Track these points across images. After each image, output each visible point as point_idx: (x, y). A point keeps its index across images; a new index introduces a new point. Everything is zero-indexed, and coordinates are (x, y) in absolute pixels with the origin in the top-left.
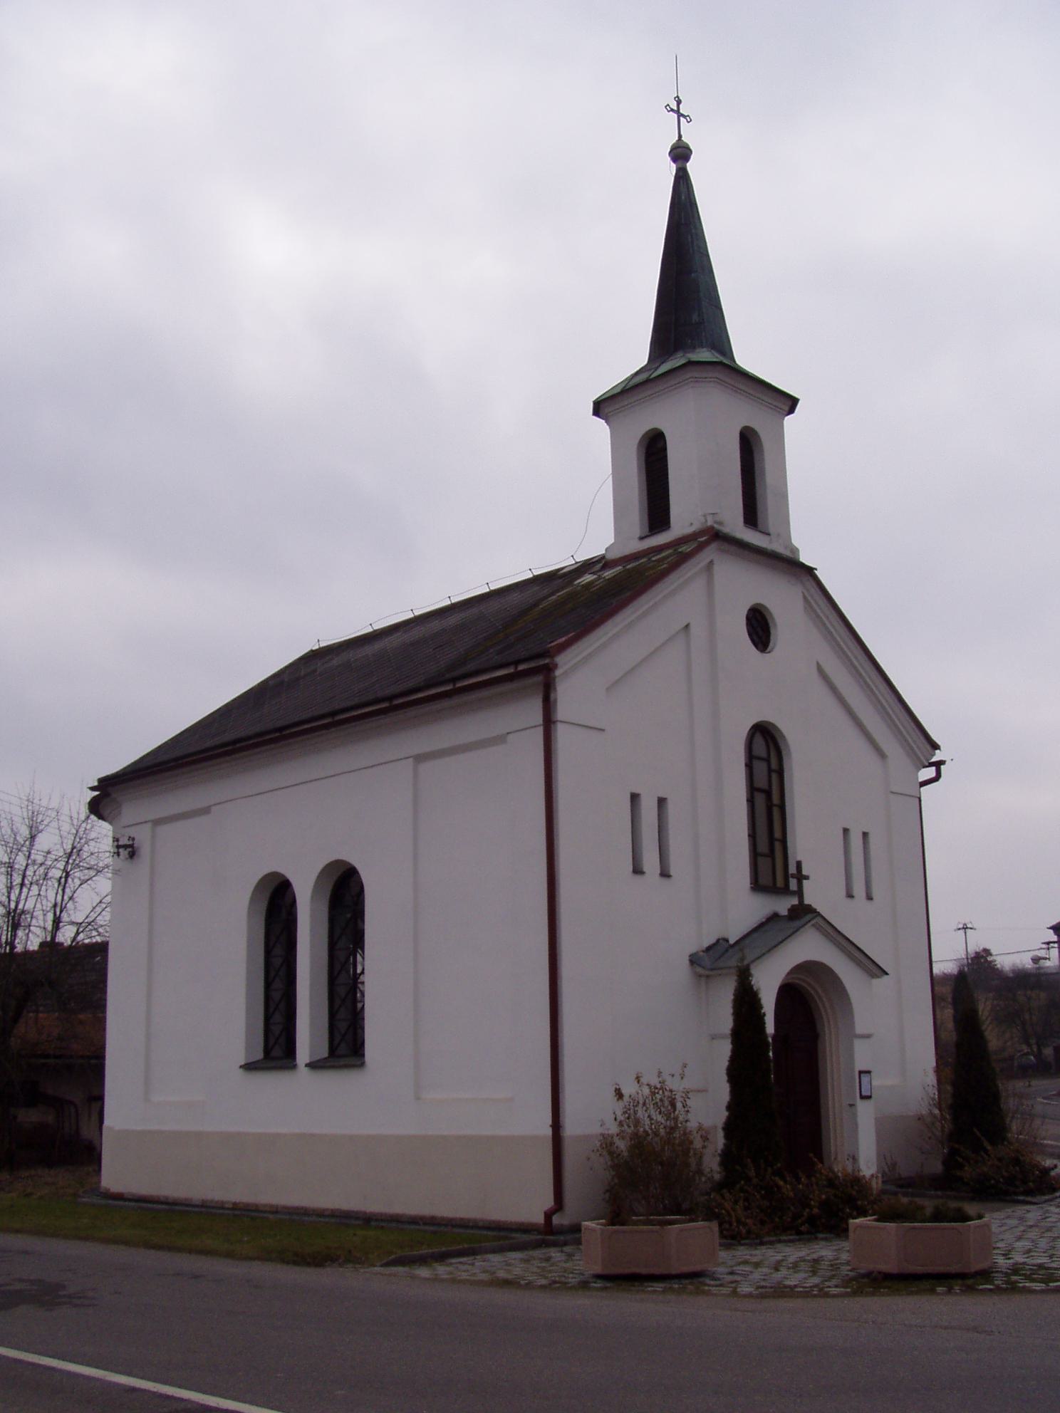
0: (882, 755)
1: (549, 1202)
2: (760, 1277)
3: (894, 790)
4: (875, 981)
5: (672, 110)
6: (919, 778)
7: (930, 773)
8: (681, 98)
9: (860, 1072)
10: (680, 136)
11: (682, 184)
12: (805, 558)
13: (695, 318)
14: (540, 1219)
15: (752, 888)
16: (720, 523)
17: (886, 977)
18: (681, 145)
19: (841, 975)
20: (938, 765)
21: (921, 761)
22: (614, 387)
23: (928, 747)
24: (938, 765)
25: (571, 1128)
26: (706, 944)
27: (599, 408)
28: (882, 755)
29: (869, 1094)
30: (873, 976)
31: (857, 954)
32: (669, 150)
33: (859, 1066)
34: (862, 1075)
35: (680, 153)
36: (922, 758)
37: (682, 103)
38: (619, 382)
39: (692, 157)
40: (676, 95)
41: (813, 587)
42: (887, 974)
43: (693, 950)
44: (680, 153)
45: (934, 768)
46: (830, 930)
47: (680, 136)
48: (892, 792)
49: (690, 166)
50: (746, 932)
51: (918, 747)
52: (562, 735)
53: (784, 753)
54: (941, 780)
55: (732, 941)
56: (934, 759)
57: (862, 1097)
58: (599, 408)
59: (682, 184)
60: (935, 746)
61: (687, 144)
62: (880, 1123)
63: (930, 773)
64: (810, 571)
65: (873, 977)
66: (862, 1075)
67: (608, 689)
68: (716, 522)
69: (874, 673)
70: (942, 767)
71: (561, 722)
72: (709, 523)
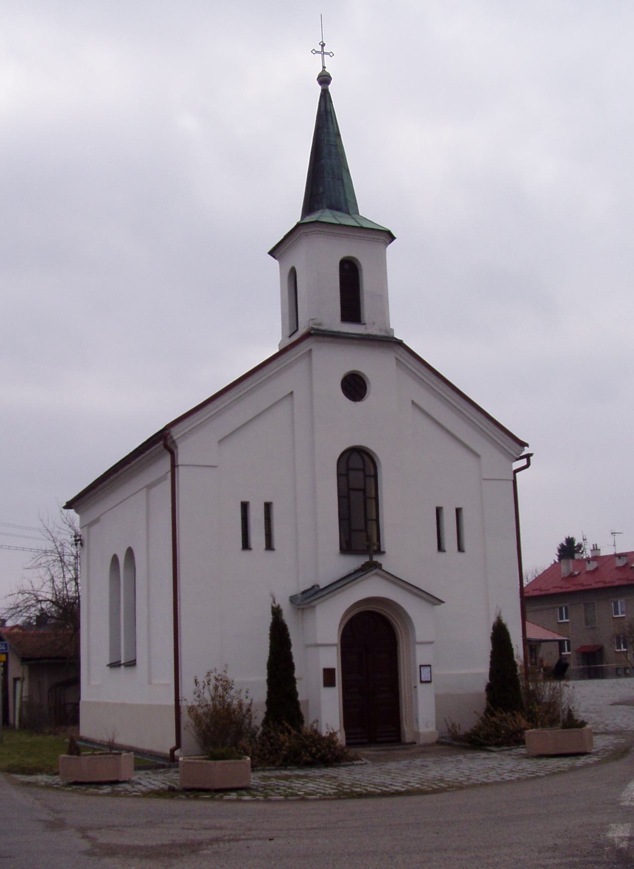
0: (477, 455)
1: (173, 743)
2: (537, 768)
3: (485, 477)
4: (436, 607)
5: (317, 52)
6: (513, 467)
7: (523, 462)
8: (324, 42)
9: (421, 666)
10: (324, 67)
11: (325, 97)
12: (397, 336)
13: (321, 190)
14: (168, 752)
15: (340, 553)
16: (320, 324)
17: (443, 604)
18: (324, 74)
19: (403, 605)
20: (528, 456)
21: (514, 457)
22: (366, 219)
23: (518, 447)
24: (528, 456)
25: (183, 704)
26: (303, 589)
27: (272, 253)
28: (477, 455)
29: (429, 680)
30: (435, 604)
31: (415, 591)
32: (317, 77)
33: (420, 660)
34: (422, 668)
35: (324, 80)
36: (513, 453)
37: (326, 46)
38: (364, 216)
39: (332, 81)
40: (321, 40)
41: (404, 353)
42: (444, 602)
43: (294, 593)
44: (324, 80)
45: (525, 460)
46: (388, 576)
47: (324, 67)
48: (485, 479)
49: (331, 88)
50: (338, 579)
51: (509, 447)
52: (181, 472)
53: (377, 465)
54: (530, 467)
55: (322, 587)
56: (524, 453)
57: (422, 682)
58: (272, 253)
59: (325, 97)
60: (523, 445)
61: (329, 74)
62: (438, 698)
63: (523, 462)
64: (400, 343)
65: (434, 605)
66: (422, 668)
67: (219, 442)
68: (315, 324)
69: (462, 401)
70: (531, 458)
71: (182, 465)
72: (311, 326)
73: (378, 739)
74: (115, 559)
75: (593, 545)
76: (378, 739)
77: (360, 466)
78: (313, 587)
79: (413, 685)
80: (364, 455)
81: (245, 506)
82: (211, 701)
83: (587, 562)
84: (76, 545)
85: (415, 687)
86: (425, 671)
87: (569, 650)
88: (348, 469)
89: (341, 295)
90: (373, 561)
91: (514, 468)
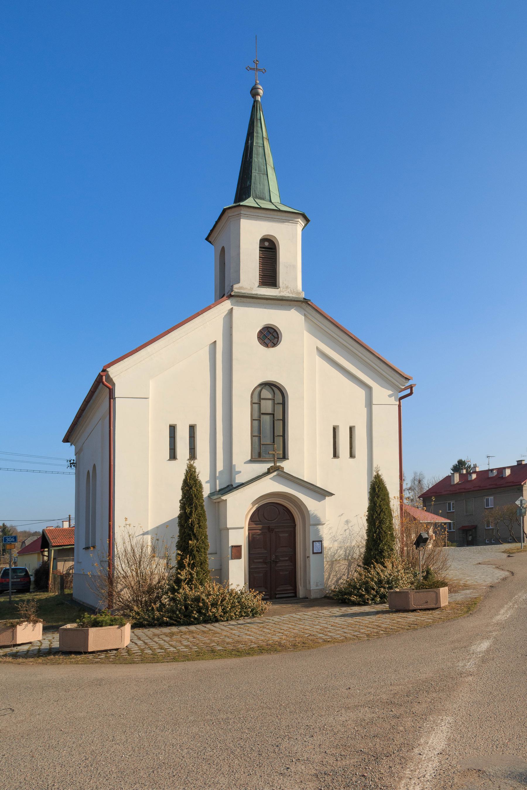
9: (313, 542)
20: (411, 387)
23: (404, 380)
57: (313, 553)
60: (407, 379)
63: (408, 391)
73: (277, 596)
74: (88, 472)
75: (474, 465)
76: (277, 596)
77: (270, 396)
78: (228, 486)
79: (307, 555)
80: (272, 387)
81: (173, 429)
82: (344, 556)
83: (469, 475)
84: (71, 466)
85: (308, 557)
86: (317, 544)
87: (453, 529)
88: (260, 399)
89: (356, 367)
90: (276, 466)
91: (229, 215)
